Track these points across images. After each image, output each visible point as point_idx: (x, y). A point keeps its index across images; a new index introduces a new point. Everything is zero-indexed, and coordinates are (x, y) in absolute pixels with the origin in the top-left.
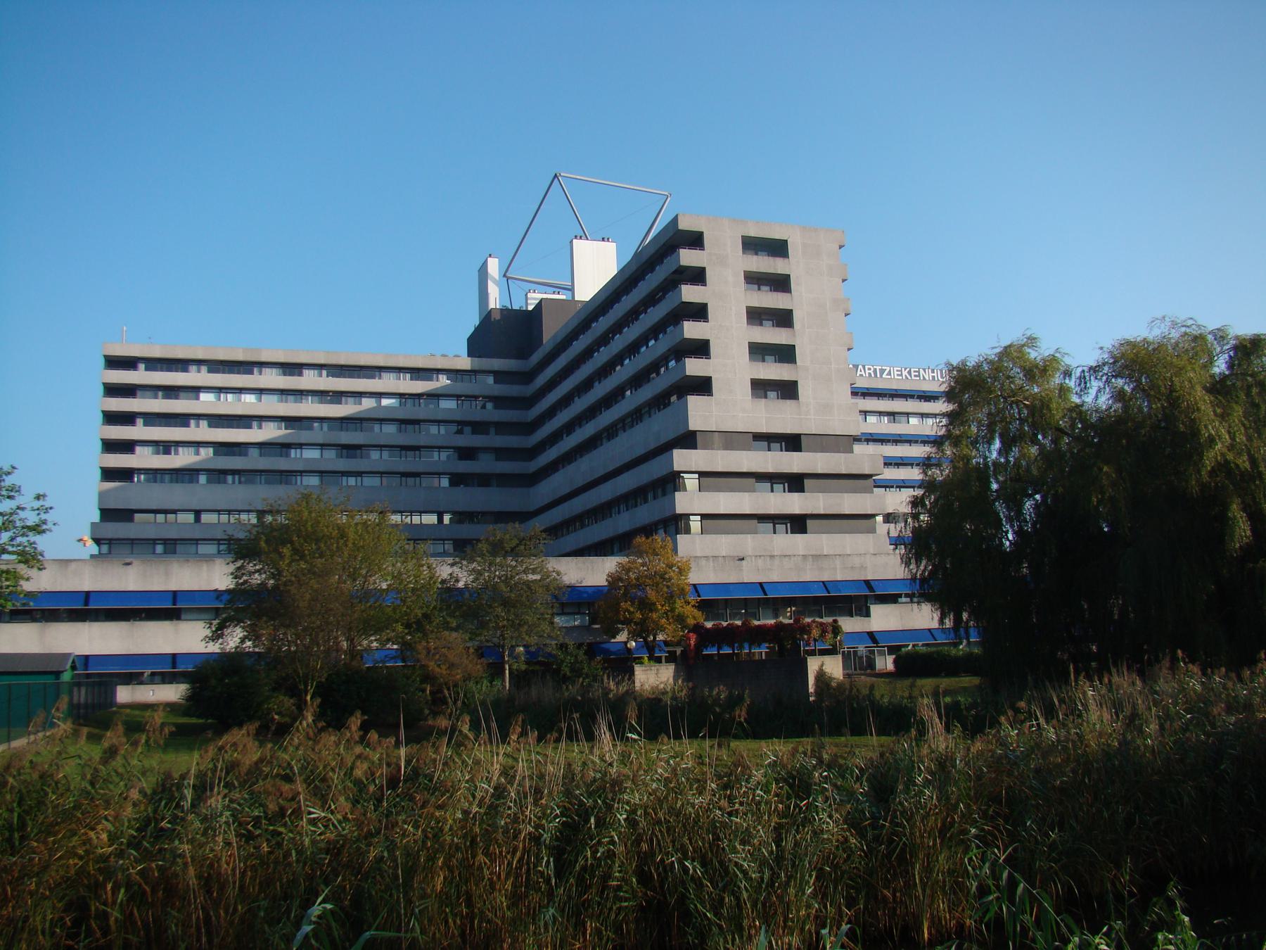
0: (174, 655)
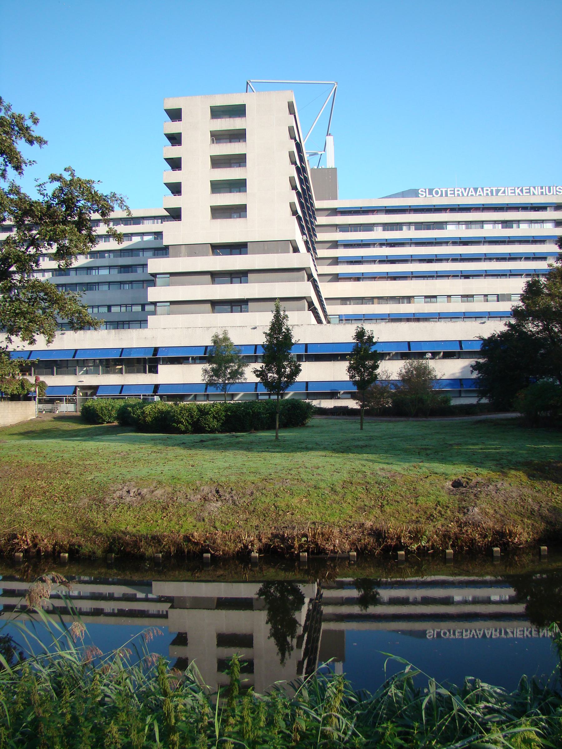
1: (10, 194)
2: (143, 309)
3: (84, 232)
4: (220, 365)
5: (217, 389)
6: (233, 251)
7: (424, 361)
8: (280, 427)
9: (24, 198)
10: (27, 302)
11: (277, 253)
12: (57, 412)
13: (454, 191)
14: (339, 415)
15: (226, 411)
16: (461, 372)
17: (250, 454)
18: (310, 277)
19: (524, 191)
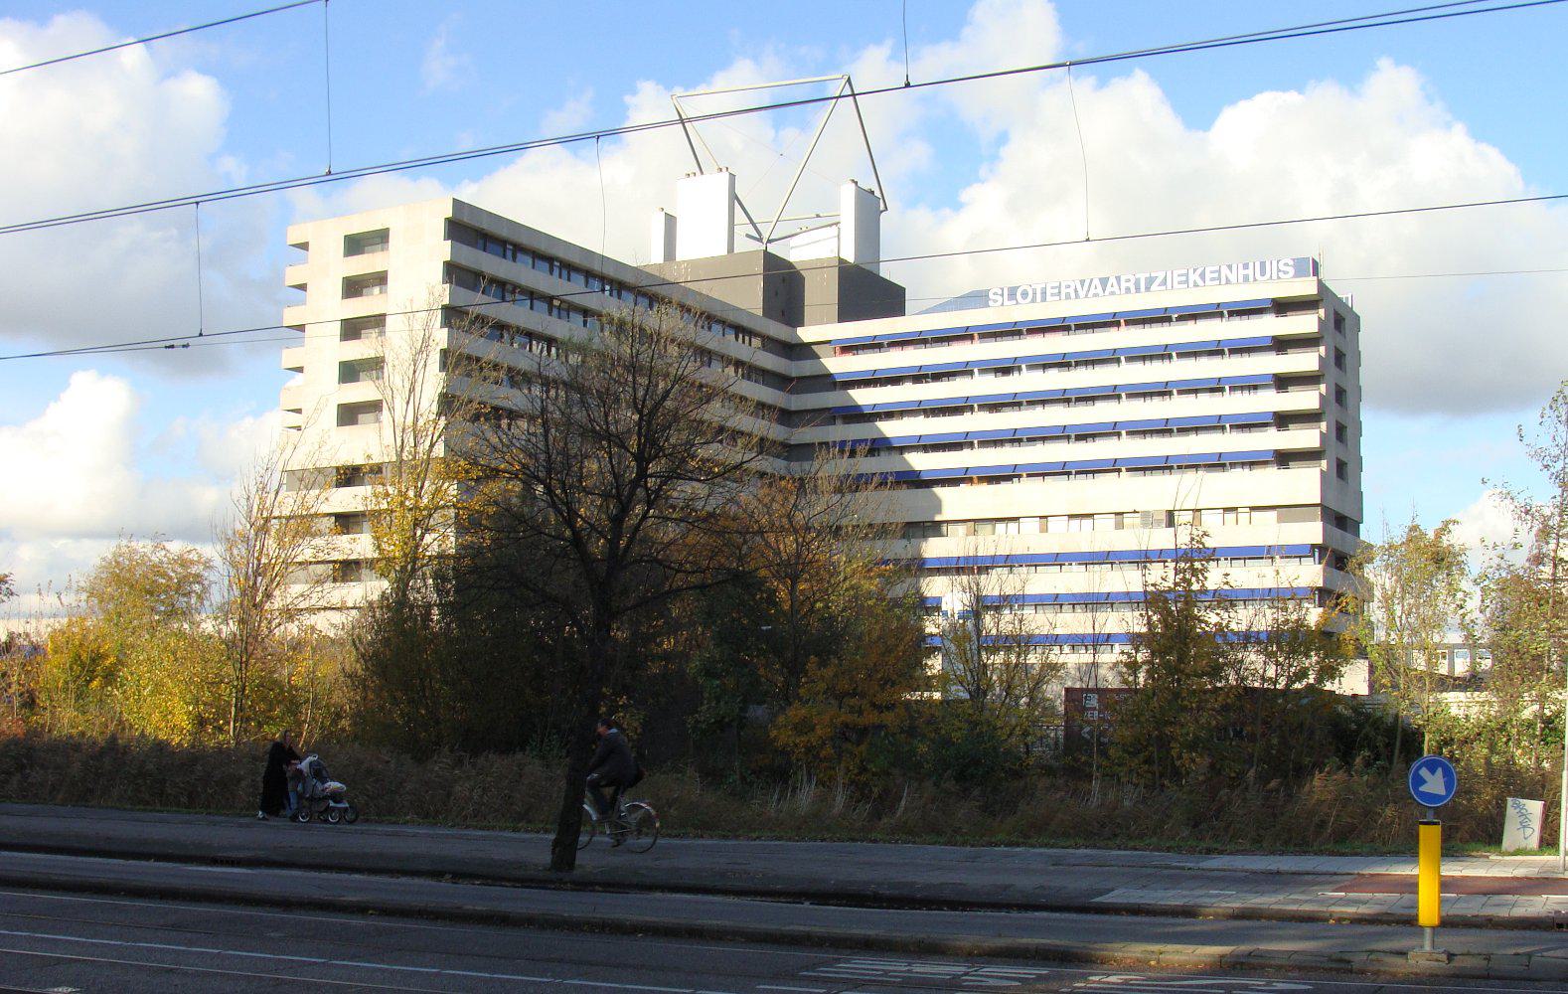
19: (1208, 276)
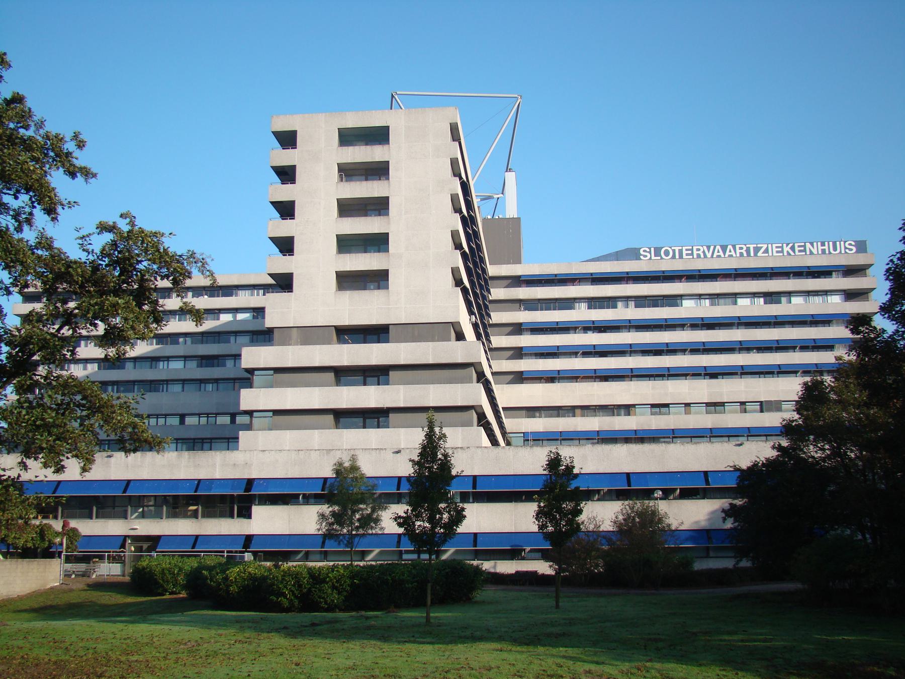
0: (475, 534)
1: (37, 249)
2: (233, 421)
3: (146, 307)
4: (344, 508)
5: (339, 544)
6: (369, 337)
7: (652, 503)
8: (433, 603)
9: (59, 256)
10: (55, 409)
11: (433, 341)
12: (94, 576)
13: (692, 250)
14: (523, 585)
15: (352, 577)
16: (709, 519)
17: (386, 646)
18: (481, 376)
19: (797, 249)
